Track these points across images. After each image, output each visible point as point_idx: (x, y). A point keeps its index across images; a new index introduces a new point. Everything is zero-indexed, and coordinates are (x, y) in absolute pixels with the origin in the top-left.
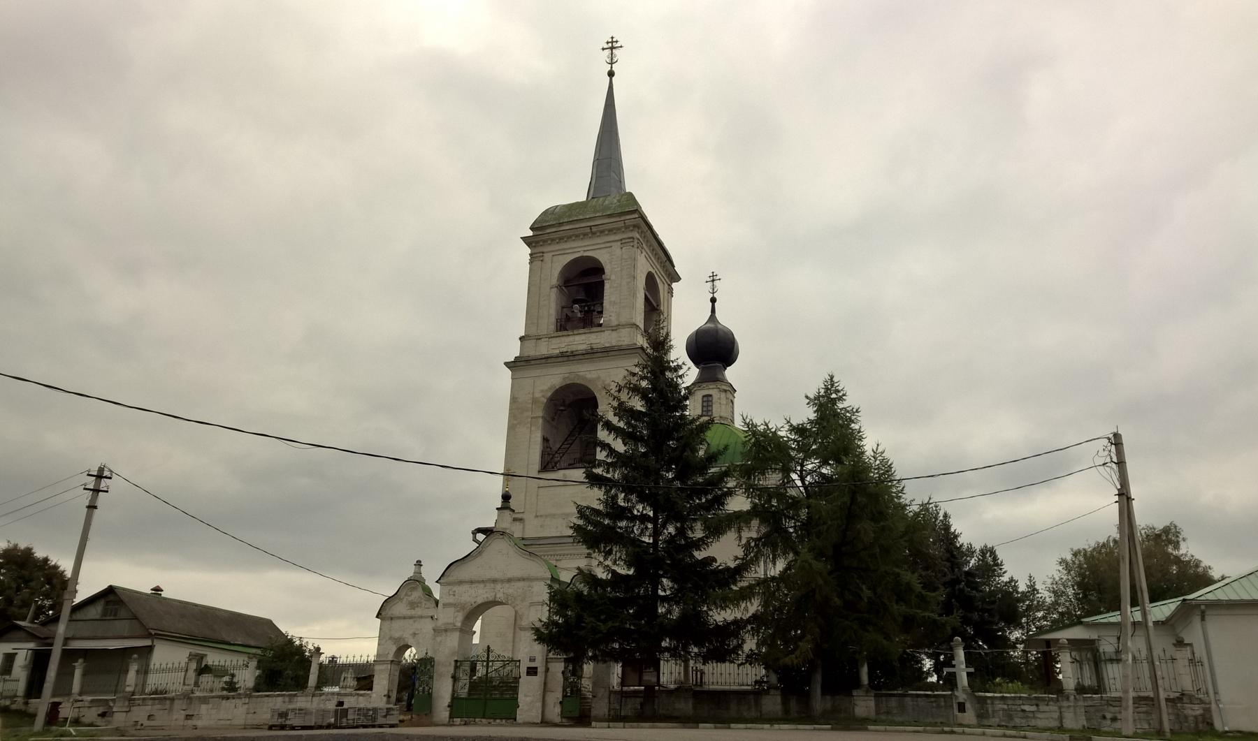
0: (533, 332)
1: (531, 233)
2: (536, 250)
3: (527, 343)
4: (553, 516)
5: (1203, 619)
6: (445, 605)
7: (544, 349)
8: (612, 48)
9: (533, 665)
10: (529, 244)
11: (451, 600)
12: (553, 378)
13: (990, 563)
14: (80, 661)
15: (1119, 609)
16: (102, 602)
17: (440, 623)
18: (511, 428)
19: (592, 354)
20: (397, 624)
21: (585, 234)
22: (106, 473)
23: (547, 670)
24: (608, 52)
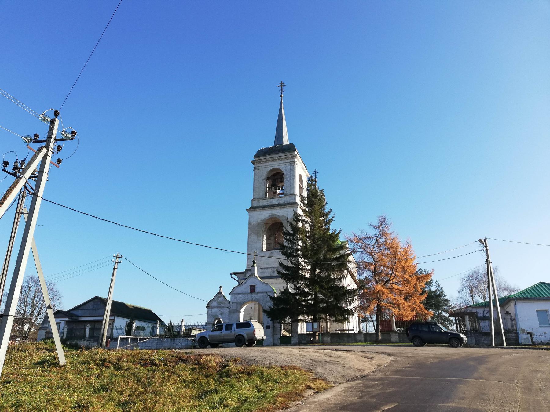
0: (256, 197)
1: (254, 159)
2: (256, 166)
3: (254, 201)
4: (267, 268)
5: (515, 304)
6: (233, 303)
7: (262, 203)
8: (282, 86)
9: (269, 325)
10: (253, 163)
11: (235, 301)
12: (265, 214)
13: (265, 218)
14: (88, 325)
15: (281, 343)
16: (92, 302)
17: (231, 309)
18: (249, 235)
19: (279, 205)
20: (214, 310)
21: (276, 160)
22: (119, 256)
23: (274, 327)
24: (280, 87)
